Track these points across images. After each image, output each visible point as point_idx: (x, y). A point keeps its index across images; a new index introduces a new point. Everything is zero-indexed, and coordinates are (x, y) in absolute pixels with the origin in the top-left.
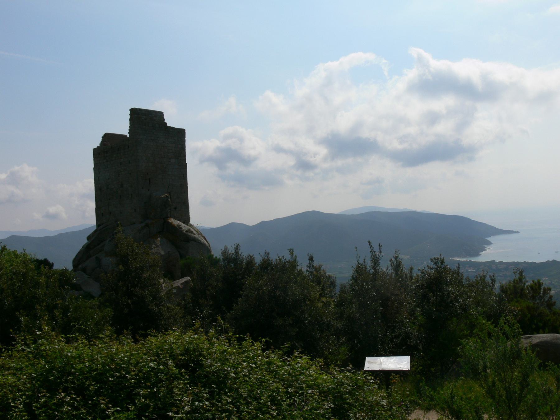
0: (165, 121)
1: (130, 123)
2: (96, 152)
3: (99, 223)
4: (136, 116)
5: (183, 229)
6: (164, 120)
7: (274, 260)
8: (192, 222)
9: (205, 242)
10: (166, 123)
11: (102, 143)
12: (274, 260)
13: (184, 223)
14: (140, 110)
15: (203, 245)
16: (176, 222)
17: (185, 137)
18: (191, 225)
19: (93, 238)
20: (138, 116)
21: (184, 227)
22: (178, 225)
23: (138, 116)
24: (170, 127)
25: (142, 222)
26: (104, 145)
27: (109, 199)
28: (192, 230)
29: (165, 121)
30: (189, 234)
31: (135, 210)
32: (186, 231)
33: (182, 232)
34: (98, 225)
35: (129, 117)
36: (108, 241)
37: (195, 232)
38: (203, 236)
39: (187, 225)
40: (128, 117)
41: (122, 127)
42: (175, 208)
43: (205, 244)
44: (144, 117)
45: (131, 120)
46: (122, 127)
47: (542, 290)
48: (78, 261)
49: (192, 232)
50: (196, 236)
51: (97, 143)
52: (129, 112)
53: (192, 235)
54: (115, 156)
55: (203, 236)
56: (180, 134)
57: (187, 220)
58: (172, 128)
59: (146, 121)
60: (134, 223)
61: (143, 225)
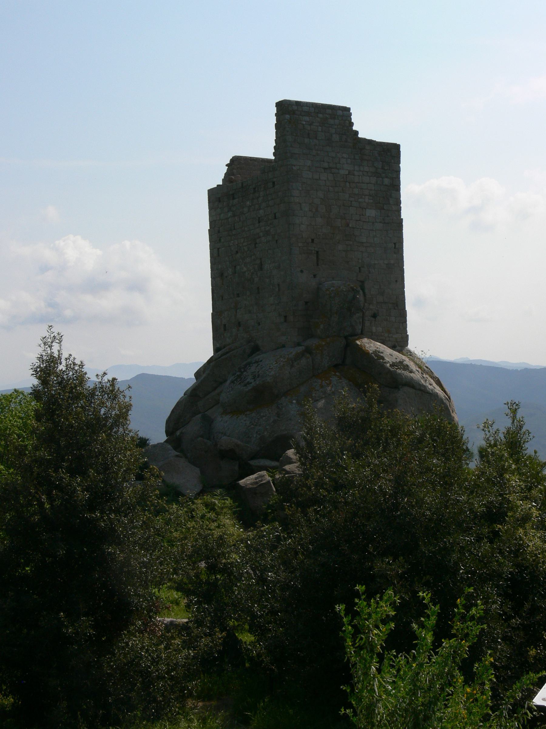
0: (354, 128)
1: (277, 133)
2: (215, 196)
3: (218, 346)
4: (287, 116)
5: (387, 359)
6: (352, 124)
7: (88, 385)
8: (411, 346)
9: (438, 390)
10: (357, 133)
11: (228, 177)
12: (88, 385)
13: (393, 347)
14: (298, 103)
15: (433, 396)
16: (370, 345)
17: (399, 162)
18: (410, 354)
19: (204, 375)
20: (292, 117)
21: (389, 355)
22: (376, 352)
23: (292, 117)
24: (365, 140)
25: (299, 344)
26: (231, 181)
27: (238, 295)
28: (407, 361)
29: (354, 128)
30: (399, 371)
31: (286, 317)
32: (393, 365)
33: (383, 366)
34: (216, 350)
35: (274, 120)
36: (228, 382)
37: (413, 367)
38: (433, 378)
39: (400, 351)
40: (273, 120)
41: (262, 145)
42: (374, 316)
43: (436, 395)
44: (307, 118)
45: (278, 126)
46: (262, 145)
47: (219, 353)
48: (175, 423)
49: (406, 368)
50: (417, 376)
51: (217, 179)
52: (274, 110)
53: (406, 373)
54: (248, 203)
55: (433, 378)
56: (387, 156)
57: (400, 341)
58: (370, 142)
59: (312, 128)
60: (284, 346)
61: (300, 349)
